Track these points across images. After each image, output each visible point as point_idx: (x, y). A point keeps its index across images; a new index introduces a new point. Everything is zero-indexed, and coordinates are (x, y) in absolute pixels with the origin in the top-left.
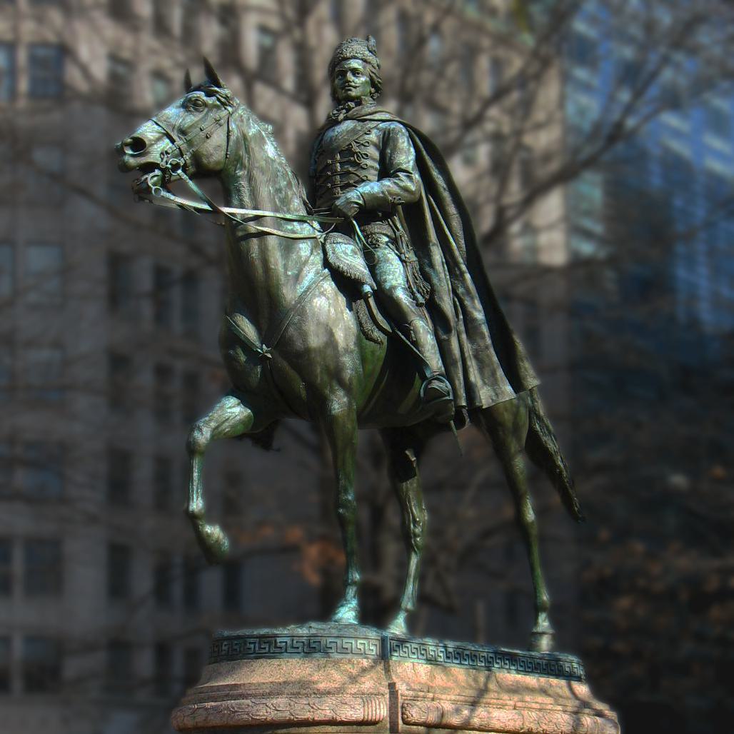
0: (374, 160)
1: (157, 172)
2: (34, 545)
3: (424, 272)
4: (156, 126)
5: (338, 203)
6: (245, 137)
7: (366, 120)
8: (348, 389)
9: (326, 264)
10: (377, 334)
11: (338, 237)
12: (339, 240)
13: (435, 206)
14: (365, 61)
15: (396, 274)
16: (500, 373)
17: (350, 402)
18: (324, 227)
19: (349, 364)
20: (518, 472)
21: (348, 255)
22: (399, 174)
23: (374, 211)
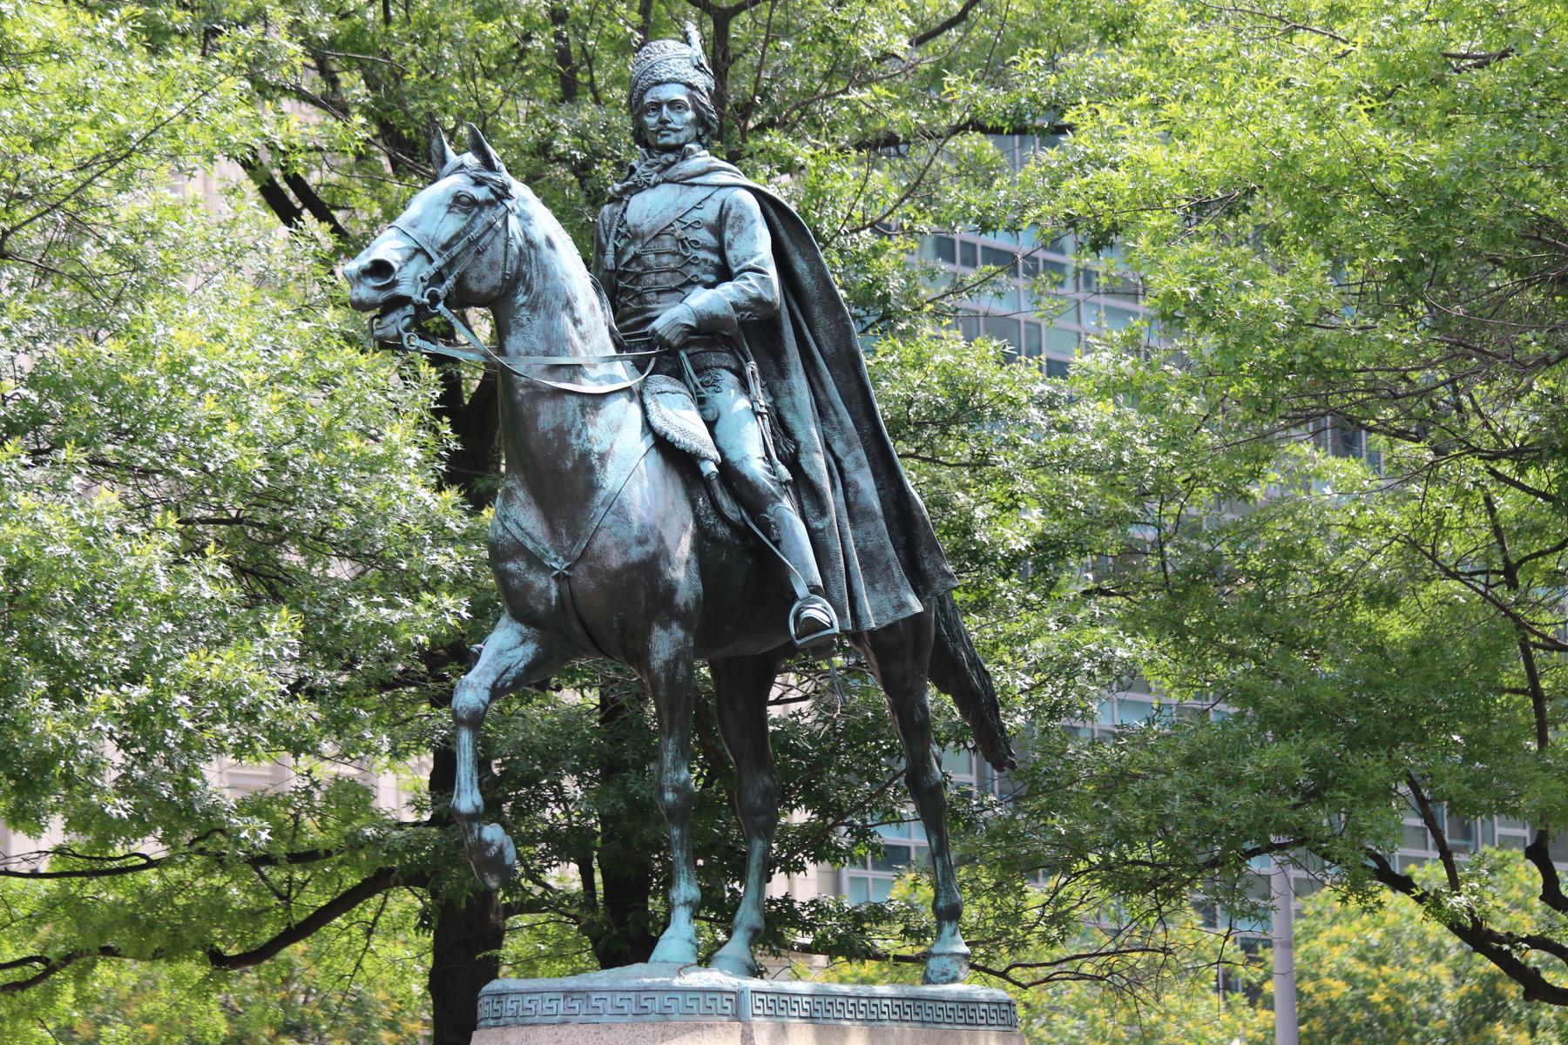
0: (709, 249)
1: (410, 310)
2: (24, 647)
3: (781, 428)
4: (405, 238)
5: (657, 324)
6: (530, 243)
7: (693, 185)
8: (684, 618)
9: (647, 425)
10: (723, 531)
11: (661, 382)
12: (666, 387)
13: (801, 319)
14: (689, 86)
15: (751, 447)
16: (898, 571)
17: (686, 639)
18: (640, 365)
19: (681, 572)
20: (809, 287)
21: (681, 420)
22: (747, 274)
23: (708, 334)
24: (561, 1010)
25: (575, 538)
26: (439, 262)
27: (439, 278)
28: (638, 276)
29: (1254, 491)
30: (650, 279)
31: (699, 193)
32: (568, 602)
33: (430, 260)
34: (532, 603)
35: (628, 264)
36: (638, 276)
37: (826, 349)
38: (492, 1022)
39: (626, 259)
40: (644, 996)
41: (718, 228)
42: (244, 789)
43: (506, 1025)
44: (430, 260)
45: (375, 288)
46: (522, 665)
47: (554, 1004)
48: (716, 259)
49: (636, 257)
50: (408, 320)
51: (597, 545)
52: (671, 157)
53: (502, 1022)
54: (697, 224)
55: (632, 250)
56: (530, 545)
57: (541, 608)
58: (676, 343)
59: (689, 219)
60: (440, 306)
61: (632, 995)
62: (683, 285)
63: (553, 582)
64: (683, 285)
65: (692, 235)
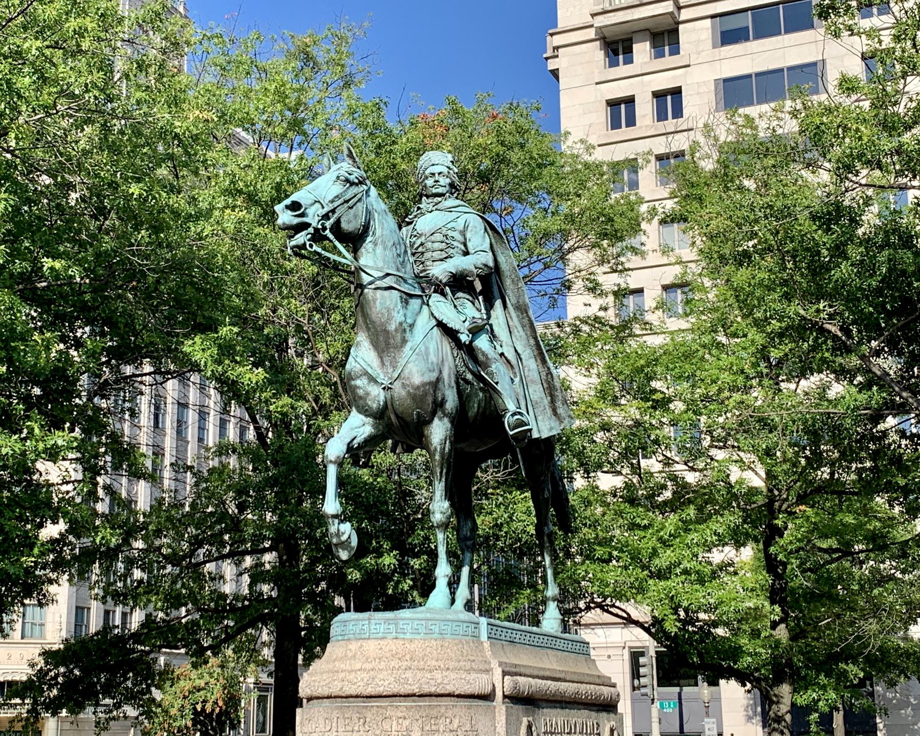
1: (311, 230)
24: (382, 630)
26: (326, 209)
27: (326, 217)
28: (423, 253)
29: (602, 509)
30: (428, 255)
31: (454, 215)
32: (389, 404)
33: (323, 207)
34: (369, 403)
35: (417, 249)
36: (423, 253)
37: (512, 301)
38: (340, 638)
39: (416, 246)
40: (430, 623)
41: (463, 233)
42: (442, 342)
43: (349, 640)
44: (323, 207)
45: (295, 216)
46: (363, 437)
47: (378, 626)
48: (463, 248)
49: (422, 244)
50: (309, 236)
51: (406, 371)
52: (440, 199)
53: (346, 638)
54: (453, 229)
55: (418, 242)
56: (370, 371)
57: (375, 406)
58: (444, 281)
59: (449, 226)
60: (327, 232)
61: (423, 622)
62: (446, 258)
63: (382, 391)
64: (446, 258)
65: (450, 233)
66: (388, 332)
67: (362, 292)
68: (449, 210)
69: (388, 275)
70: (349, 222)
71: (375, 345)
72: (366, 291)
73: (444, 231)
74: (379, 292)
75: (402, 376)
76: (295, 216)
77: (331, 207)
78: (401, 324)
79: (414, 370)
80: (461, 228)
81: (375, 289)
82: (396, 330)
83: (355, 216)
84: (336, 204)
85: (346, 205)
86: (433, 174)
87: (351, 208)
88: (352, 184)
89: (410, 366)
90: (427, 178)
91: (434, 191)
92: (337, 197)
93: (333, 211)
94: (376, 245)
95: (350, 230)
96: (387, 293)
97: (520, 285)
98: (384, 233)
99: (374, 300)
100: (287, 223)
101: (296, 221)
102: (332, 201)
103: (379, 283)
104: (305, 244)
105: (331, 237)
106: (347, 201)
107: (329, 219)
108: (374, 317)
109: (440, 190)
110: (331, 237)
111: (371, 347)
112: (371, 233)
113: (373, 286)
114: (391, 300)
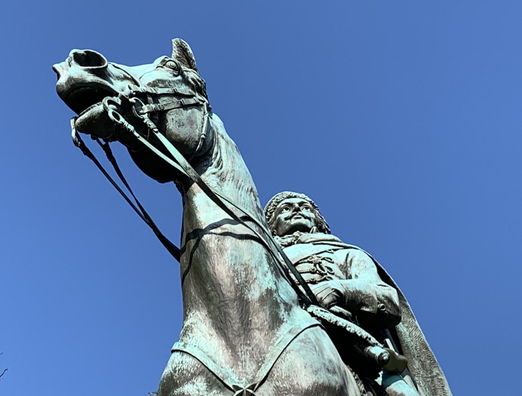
25: (259, 364)
51: (283, 367)
59: (323, 255)
66: (247, 302)
67: (199, 240)
68: (315, 243)
69: (248, 218)
70: (181, 124)
71: (220, 325)
72: (206, 237)
73: (315, 259)
74: (229, 241)
75: (275, 373)
76: (92, 71)
77: (149, 90)
78: (269, 292)
79: (299, 363)
80: (342, 261)
81: (221, 234)
82: (262, 300)
83: (191, 122)
84: (160, 91)
85: (175, 99)
86: (290, 205)
87: (185, 107)
88: (185, 81)
89: (289, 357)
90: (280, 211)
91: (293, 222)
92: (162, 81)
93: (156, 97)
94: (223, 180)
95: (182, 136)
96: (244, 244)
97: (435, 371)
98: (236, 169)
99: (221, 251)
100: (76, 76)
101: (90, 78)
102: (154, 84)
103: (228, 227)
104: (105, 111)
105: (152, 125)
106: (176, 95)
107: (146, 103)
108: (216, 286)
109: (303, 221)
110: (152, 125)
111: (213, 332)
112: (215, 163)
113: (219, 230)
114: (252, 254)
